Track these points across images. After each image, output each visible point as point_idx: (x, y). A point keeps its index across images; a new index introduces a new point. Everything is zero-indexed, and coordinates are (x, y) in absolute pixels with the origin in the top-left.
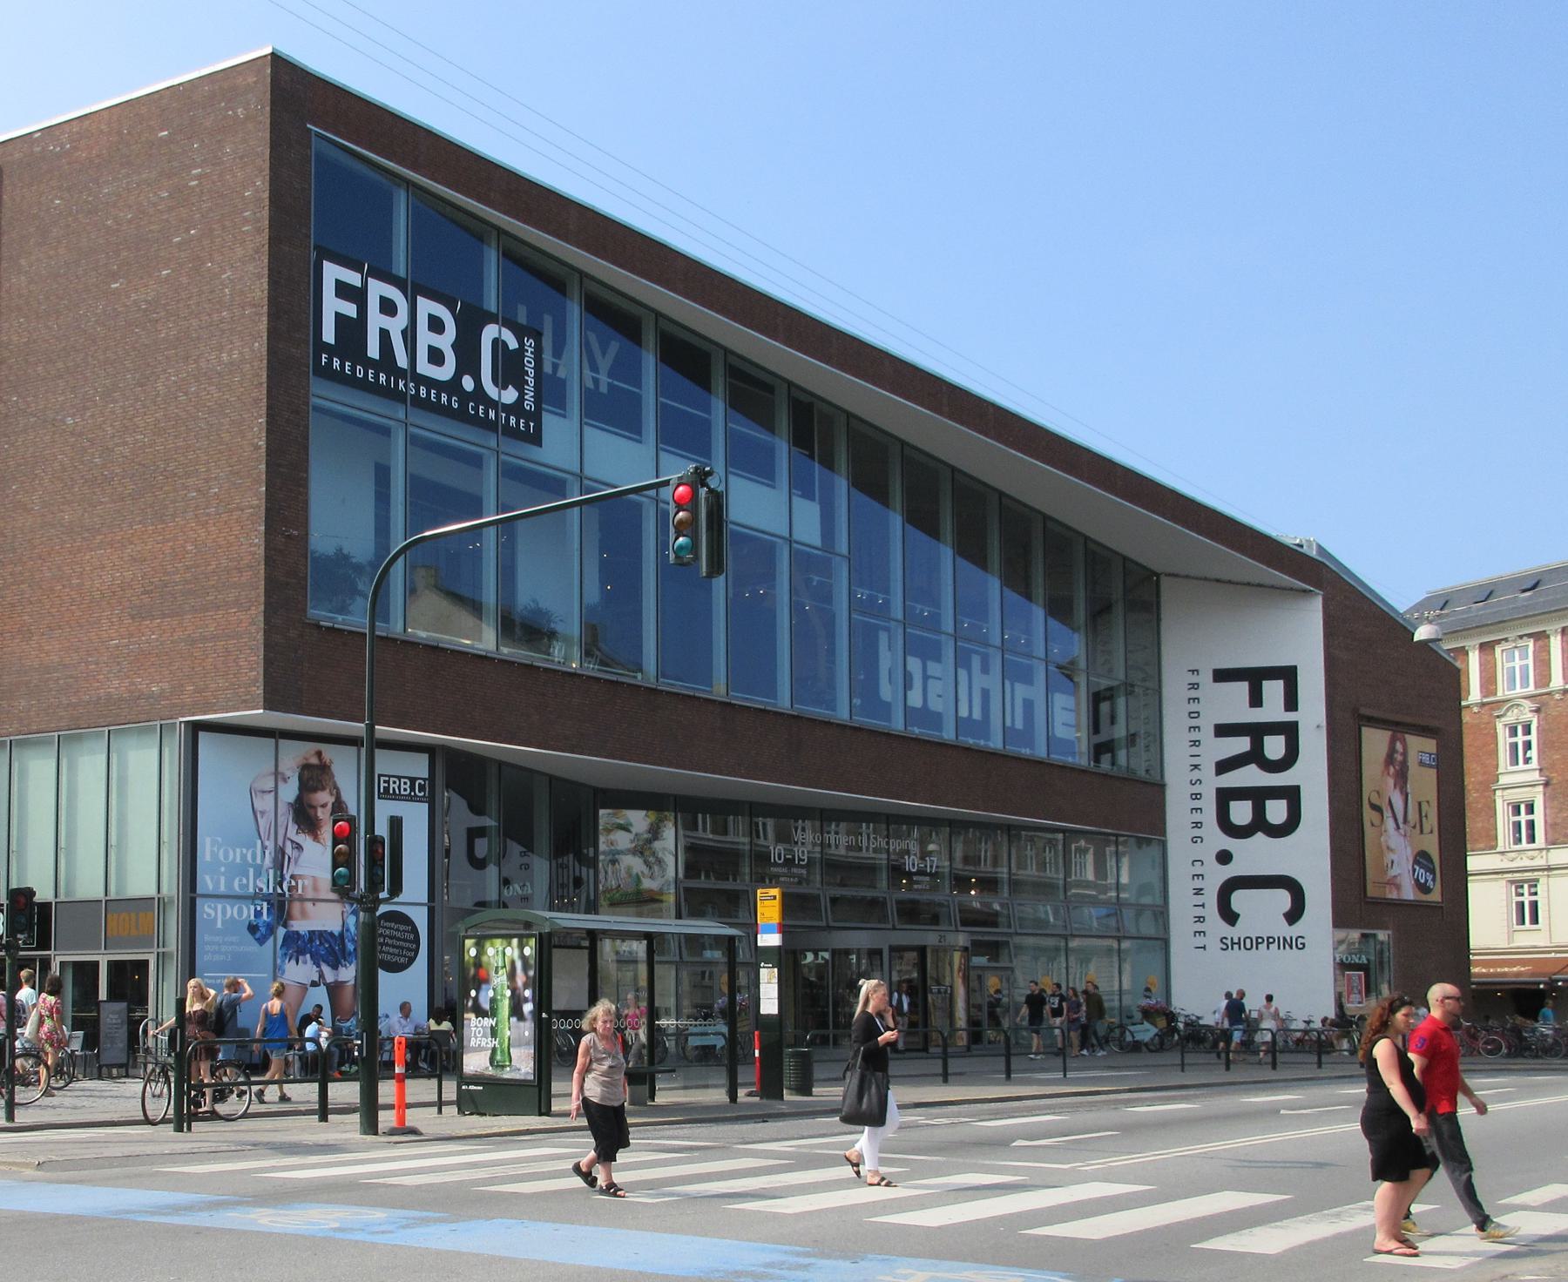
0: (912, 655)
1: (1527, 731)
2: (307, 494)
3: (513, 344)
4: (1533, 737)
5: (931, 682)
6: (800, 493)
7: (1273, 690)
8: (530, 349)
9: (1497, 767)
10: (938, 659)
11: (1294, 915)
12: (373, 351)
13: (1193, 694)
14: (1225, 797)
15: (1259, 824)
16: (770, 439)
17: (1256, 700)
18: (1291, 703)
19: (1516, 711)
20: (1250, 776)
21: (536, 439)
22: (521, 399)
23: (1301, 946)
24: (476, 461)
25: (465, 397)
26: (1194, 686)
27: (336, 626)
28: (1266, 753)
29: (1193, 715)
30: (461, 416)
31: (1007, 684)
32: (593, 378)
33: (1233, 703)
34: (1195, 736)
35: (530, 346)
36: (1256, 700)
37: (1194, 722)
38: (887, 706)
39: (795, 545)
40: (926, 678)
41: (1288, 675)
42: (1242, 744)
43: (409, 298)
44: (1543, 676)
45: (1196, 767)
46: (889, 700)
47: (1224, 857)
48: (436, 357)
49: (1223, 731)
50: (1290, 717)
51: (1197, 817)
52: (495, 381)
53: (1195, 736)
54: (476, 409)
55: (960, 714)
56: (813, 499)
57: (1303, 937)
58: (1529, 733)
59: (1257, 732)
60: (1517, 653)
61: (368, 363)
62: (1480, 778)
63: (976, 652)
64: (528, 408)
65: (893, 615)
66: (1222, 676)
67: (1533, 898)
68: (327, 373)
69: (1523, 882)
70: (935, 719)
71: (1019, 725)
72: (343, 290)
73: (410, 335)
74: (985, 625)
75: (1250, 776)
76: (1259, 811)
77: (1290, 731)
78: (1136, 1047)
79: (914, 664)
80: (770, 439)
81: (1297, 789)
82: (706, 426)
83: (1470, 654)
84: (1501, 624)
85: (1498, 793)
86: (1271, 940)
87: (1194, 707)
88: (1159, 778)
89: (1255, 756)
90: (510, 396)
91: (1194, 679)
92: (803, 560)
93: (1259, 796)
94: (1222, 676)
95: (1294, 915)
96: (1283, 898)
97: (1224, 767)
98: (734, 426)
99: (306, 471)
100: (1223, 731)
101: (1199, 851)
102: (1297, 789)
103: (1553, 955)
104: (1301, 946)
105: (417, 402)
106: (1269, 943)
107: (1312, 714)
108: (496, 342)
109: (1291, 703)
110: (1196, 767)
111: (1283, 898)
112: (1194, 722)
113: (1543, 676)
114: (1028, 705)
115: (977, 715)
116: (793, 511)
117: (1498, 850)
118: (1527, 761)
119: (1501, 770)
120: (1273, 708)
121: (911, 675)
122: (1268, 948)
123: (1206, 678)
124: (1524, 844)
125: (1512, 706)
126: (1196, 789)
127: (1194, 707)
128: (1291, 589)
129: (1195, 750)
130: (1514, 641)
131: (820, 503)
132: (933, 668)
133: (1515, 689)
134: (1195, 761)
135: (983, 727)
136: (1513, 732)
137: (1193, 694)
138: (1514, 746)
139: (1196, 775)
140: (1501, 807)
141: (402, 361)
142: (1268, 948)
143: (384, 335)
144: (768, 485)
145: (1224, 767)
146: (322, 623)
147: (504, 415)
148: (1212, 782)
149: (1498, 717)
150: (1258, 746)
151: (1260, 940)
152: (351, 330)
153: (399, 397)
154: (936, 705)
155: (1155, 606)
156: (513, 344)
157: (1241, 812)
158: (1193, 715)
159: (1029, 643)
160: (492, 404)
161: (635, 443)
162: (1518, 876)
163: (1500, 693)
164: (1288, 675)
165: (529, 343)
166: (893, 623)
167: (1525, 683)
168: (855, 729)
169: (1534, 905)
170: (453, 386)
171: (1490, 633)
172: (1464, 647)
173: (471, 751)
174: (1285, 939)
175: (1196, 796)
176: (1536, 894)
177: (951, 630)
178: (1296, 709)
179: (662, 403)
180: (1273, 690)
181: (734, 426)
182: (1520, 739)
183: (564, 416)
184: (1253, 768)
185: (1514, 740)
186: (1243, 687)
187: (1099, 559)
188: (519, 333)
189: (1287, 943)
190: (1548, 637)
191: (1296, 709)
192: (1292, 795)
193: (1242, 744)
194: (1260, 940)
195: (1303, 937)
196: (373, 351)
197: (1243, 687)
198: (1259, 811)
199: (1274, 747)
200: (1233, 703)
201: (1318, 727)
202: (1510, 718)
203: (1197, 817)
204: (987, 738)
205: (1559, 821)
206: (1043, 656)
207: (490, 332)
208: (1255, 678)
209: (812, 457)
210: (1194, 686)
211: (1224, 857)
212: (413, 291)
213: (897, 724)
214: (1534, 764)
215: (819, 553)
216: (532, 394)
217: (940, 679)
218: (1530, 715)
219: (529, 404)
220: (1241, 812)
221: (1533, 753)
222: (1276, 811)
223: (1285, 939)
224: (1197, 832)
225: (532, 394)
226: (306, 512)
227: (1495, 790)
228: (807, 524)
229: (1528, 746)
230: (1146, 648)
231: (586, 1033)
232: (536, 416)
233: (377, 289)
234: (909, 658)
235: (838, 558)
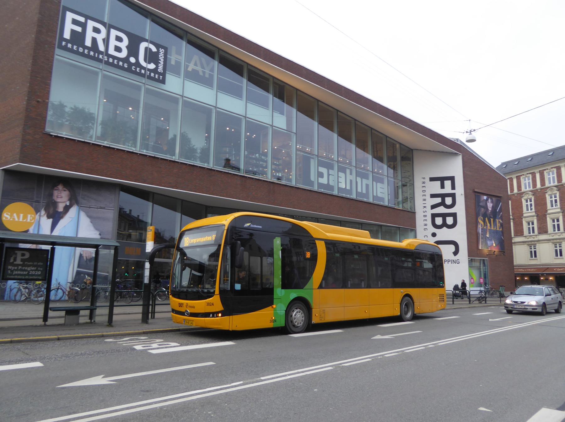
0: (358, 177)
1: (531, 201)
2: (49, 88)
3: (154, 49)
4: (533, 203)
5: (330, 176)
6: (279, 113)
7: (448, 183)
8: (162, 52)
9: (522, 211)
10: (333, 169)
11: (456, 253)
12: (88, 43)
13: (424, 185)
14: (434, 216)
15: (444, 224)
16: (267, 95)
17: (443, 187)
18: (453, 187)
19: (527, 195)
20: (441, 210)
21: (163, 82)
22: (157, 68)
23: (458, 263)
24: (139, 88)
25: (130, 64)
26: (424, 183)
27: (195, 164)
28: (449, 204)
29: (423, 191)
30: (129, 70)
31: (374, 183)
32: (203, 71)
33: (436, 188)
34: (424, 197)
35: (162, 51)
36: (443, 187)
37: (424, 194)
38: (313, 182)
39: (274, 128)
40: (329, 175)
41: (452, 179)
42: (439, 200)
43: (107, 29)
44: (535, 185)
45: (425, 207)
46: (313, 181)
47: (434, 235)
48: (118, 49)
49: (433, 196)
50: (453, 192)
51: (425, 222)
52: (145, 60)
53: (424, 197)
54: (136, 69)
55: (374, 195)
56: (283, 114)
57: (459, 260)
58: (531, 202)
59: (443, 196)
60: (527, 178)
61: (85, 47)
62: (518, 215)
63: (349, 168)
64: (160, 71)
65: (353, 165)
66: (432, 179)
67: (535, 250)
68: (65, 48)
69: (532, 244)
70: (332, 188)
71: (364, 192)
72: (75, 22)
73: (106, 41)
74: (291, 142)
75: (441, 210)
76: (444, 221)
77: (453, 196)
78: (20, 301)
79: (359, 179)
80: (267, 95)
81: (456, 213)
82: (242, 87)
83: (514, 179)
84: (522, 170)
85: (523, 219)
86: (449, 261)
87: (424, 189)
88: (413, 210)
89: (443, 204)
90: (152, 66)
91: (424, 180)
92: (277, 133)
93: (444, 216)
94: (432, 179)
95: (456, 253)
96: (452, 248)
97: (433, 207)
98: (187, 64)
99: (50, 80)
100: (433, 196)
101: (426, 233)
102: (456, 213)
103: (541, 267)
104: (458, 263)
105: (107, 63)
106: (448, 262)
107: (460, 191)
108: (146, 49)
109: (453, 187)
110: (425, 207)
111: (452, 248)
112: (424, 194)
113: (535, 185)
114: (367, 186)
115: (364, 192)
116: (218, 99)
117: (524, 235)
118: (531, 209)
119: (524, 212)
120: (448, 189)
121: (357, 182)
122: (448, 263)
123: (427, 180)
124: (532, 234)
125: (526, 193)
126: (425, 214)
127: (424, 189)
128: (452, 153)
129: (424, 202)
130: (526, 175)
131: (286, 116)
132: (331, 172)
133: (527, 189)
134: (425, 205)
135: (367, 195)
136: (527, 201)
137: (424, 185)
138: (527, 205)
139: (425, 209)
140: (525, 224)
141: (102, 48)
142: (448, 263)
143: (94, 40)
144: (211, 89)
145: (433, 207)
146: (51, 134)
147: (148, 72)
148: (430, 212)
149: (522, 197)
150: (443, 200)
151: (449, 261)
152: (78, 38)
153: (100, 61)
154: (331, 183)
155: (411, 159)
156: (154, 49)
157: (439, 221)
158: (423, 191)
159: (383, 172)
160: (142, 67)
161: (211, 90)
162: (530, 243)
163: (522, 190)
164: (452, 179)
165: (162, 51)
166: (369, 172)
167: (529, 187)
168: (297, 188)
169: (535, 252)
170: (126, 60)
171: (519, 173)
172: (511, 177)
173: (124, 184)
174: (453, 261)
175: (425, 216)
176: (535, 249)
177: (354, 165)
178: (455, 189)
179: (186, 64)
180: (448, 183)
181: (187, 64)
182: (529, 203)
183: (242, 100)
184: (442, 207)
185: (527, 203)
186: (438, 183)
187: (391, 143)
188: (158, 46)
189: (454, 262)
190: (535, 173)
191: (455, 189)
192: (454, 215)
193: (439, 200)
194: (446, 261)
195: (459, 260)
196: (88, 43)
197: (438, 183)
198: (444, 221)
199: (449, 201)
200: (436, 188)
201: (462, 194)
202: (525, 197)
203: (425, 222)
204: (351, 195)
205: (541, 227)
206: (386, 175)
207: (143, 46)
208: (442, 180)
209: (284, 102)
210: (424, 183)
211: (434, 235)
212: (109, 27)
213: (316, 188)
214: (533, 210)
215: (286, 131)
216: (159, 68)
217: (333, 175)
218: (531, 196)
219: (160, 69)
220: (439, 221)
221: (533, 207)
222: (450, 220)
223: (453, 261)
224: (425, 227)
225: (159, 68)
226: (49, 94)
227: (522, 218)
228: (280, 122)
229: (531, 205)
230: (409, 171)
231: (20, 287)
232: (164, 75)
233: (91, 24)
234: (357, 178)
235: (293, 134)
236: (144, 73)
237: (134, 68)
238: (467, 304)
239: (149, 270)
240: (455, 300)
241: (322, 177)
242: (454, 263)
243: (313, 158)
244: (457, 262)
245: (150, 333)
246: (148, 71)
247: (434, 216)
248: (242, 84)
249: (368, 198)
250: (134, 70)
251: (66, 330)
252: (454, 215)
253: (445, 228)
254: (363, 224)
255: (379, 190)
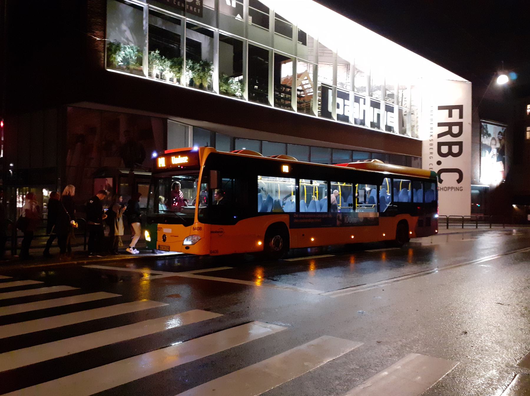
10: (348, 99)
14: (440, 145)
20: (448, 138)
36: (450, 115)
42: (446, 129)
47: (439, 163)
49: (440, 125)
59: (450, 125)
64: (197, 4)
76: (450, 149)
77: (460, 125)
89: (450, 132)
96: (456, 176)
97: (440, 136)
100: (440, 125)
109: (461, 116)
111: (456, 176)
114: (379, 115)
147: (188, 6)
150: (450, 129)
174: (458, 190)
180: (456, 112)
184: (449, 136)
186: (447, 112)
192: (460, 144)
197: (447, 112)
198: (450, 149)
203: (431, 151)
223: (458, 190)
224: (431, 155)
236: (192, 10)
237: (175, 2)
238: (460, 229)
239: (315, 212)
240: (464, 224)
241: (338, 107)
242: (457, 190)
243: (331, 89)
244: (460, 189)
245: (322, 265)
246: (187, 4)
247: (440, 145)
248: (249, 8)
249: (379, 127)
250: (175, 4)
251: (464, 265)
252: (460, 144)
253: (450, 156)
254: (311, 147)
255: (389, 119)
